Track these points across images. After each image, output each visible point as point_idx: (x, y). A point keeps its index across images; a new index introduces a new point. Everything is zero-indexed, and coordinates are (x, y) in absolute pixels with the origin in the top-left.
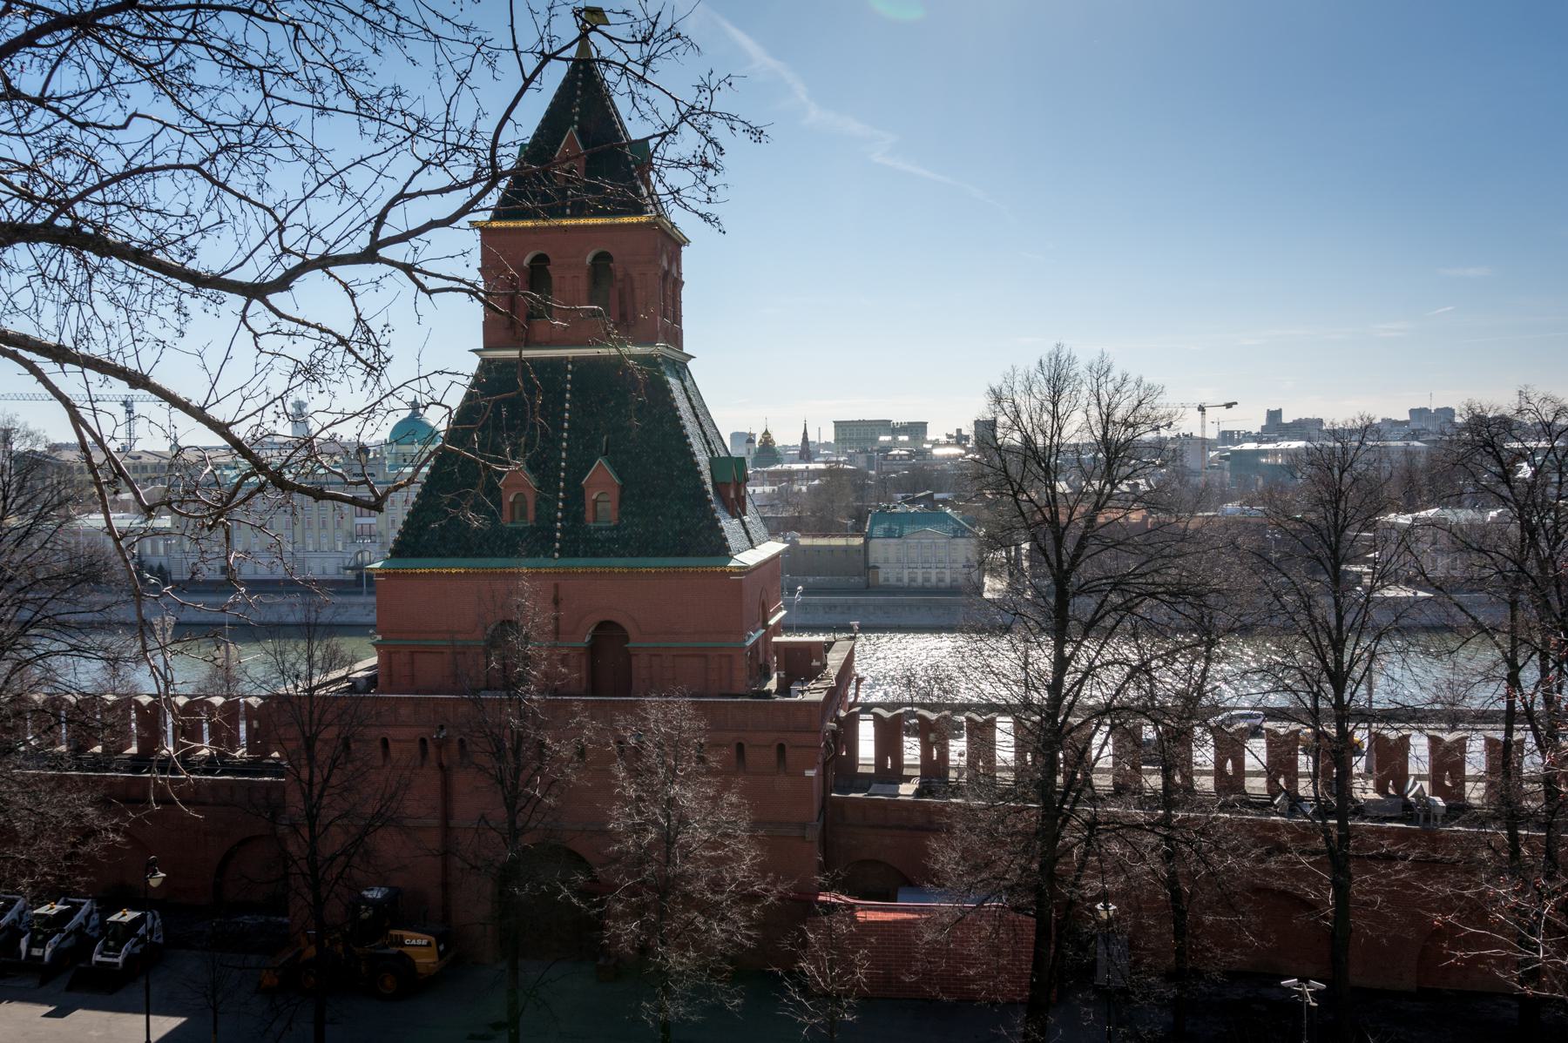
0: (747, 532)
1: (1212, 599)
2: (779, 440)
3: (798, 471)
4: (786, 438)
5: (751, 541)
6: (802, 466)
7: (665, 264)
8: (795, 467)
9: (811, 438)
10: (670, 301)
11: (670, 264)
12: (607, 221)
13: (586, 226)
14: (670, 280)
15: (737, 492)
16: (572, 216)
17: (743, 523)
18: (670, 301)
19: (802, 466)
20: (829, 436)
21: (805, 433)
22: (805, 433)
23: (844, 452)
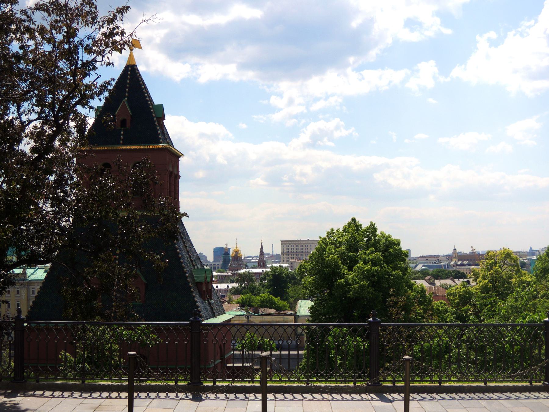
0: (212, 309)
1: (92, 35)
2: (244, 254)
3: (256, 274)
4: (249, 251)
5: (214, 313)
6: (259, 270)
7: (171, 169)
8: (255, 271)
9: (265, 251)
10: (173, 187)
11: (173, 168)
12: (109, 148)
13: (130, 150)
14: (173, 176)
15: (207, 288)
16: (125, 144)
17: (210, 304)
18: (173, 187)
19: (259, 270)
20: (278, 250)
21: (262, 248)
22: (262, 248)
23: (288, 261)
